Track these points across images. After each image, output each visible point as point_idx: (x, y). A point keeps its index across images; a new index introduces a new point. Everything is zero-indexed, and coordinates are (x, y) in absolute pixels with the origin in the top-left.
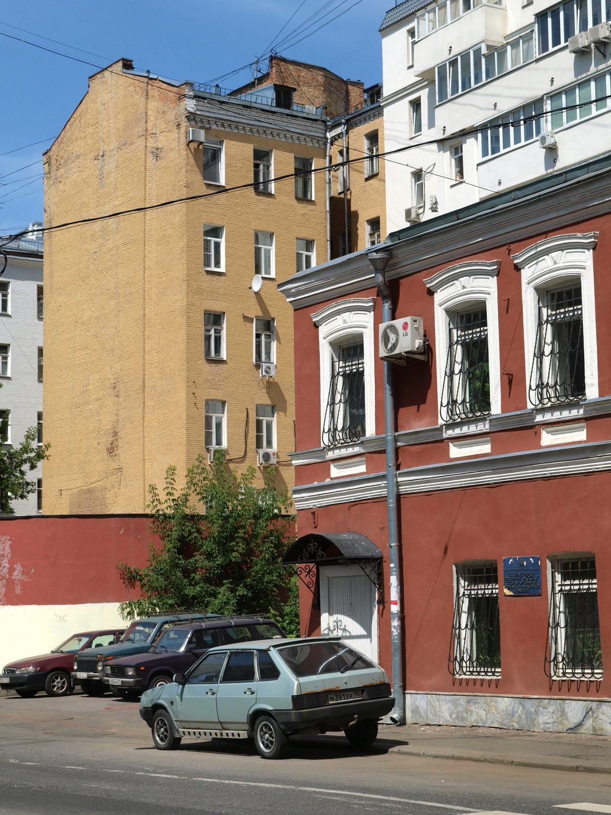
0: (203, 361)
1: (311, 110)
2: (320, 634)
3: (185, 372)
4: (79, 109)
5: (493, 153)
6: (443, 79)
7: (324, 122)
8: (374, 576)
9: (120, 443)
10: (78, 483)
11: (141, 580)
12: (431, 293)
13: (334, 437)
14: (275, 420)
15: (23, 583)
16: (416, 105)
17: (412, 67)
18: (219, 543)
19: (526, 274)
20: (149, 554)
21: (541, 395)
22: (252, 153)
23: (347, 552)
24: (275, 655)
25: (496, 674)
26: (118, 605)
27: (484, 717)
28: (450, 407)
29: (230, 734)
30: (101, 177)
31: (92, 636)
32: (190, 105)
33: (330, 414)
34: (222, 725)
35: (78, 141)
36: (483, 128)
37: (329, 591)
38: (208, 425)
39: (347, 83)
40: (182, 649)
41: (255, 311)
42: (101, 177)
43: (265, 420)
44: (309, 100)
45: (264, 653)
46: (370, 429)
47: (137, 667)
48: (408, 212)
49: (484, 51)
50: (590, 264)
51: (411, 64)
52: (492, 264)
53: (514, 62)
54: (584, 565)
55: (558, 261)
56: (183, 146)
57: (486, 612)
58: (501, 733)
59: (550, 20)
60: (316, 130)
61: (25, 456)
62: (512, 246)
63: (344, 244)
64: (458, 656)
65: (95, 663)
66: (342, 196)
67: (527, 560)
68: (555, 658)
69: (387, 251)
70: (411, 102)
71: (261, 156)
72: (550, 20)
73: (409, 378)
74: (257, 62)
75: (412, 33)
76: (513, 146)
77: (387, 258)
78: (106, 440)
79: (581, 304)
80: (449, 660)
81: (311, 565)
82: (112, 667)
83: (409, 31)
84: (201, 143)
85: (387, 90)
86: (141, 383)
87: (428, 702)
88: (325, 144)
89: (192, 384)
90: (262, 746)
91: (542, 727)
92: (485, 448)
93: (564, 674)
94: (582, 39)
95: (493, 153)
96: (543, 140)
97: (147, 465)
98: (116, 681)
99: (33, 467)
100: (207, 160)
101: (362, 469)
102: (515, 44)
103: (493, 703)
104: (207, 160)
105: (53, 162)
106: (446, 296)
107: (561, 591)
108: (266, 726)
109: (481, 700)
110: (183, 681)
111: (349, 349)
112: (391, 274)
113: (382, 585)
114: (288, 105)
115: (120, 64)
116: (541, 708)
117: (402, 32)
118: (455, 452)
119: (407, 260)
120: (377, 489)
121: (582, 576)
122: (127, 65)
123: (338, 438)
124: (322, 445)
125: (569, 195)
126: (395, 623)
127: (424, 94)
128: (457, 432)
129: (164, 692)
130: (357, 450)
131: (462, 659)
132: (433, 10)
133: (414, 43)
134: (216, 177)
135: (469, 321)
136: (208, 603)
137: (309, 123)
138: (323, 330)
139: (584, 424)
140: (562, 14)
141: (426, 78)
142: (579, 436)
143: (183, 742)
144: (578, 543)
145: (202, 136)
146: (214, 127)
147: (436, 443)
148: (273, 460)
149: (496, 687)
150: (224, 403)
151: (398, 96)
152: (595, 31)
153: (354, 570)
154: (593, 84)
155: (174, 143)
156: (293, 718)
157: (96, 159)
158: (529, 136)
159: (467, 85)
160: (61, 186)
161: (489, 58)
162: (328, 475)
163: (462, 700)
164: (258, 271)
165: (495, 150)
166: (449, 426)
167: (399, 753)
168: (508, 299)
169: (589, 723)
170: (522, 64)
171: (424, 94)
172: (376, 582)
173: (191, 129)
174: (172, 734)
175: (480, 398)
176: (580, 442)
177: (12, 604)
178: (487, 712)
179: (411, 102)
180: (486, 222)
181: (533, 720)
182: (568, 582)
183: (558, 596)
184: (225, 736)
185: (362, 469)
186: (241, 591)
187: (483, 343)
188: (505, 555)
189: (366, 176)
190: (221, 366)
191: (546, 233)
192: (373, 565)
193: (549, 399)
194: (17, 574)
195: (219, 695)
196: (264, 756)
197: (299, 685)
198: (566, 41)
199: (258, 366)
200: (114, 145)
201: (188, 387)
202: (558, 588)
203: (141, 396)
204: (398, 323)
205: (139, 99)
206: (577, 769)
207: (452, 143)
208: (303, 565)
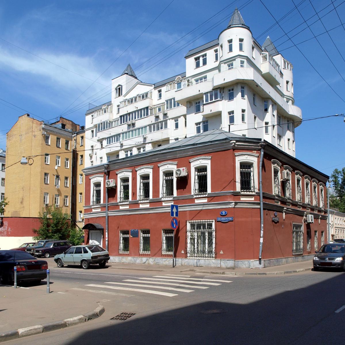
0: (44, 184)
1: (70, 130)
2: (89, 244)
3: (40, 186)
4: (16, 124)
5: (109, 144)
6: (99, 126)
7: (72, 133)
8: (102, 232)
9: (24, 201)
10: (13, 210)
11: (37, 232)
12: (117, 174)
14: (59, 198)
15: (11, 232)
16: (93, 131)
17: (92, 123)
18: (55, 225)
19: (138, 172)
20: (39, 226)
22: (56, 138)
23: (97, 227)
24: (87, 248)
25: (128, 253)
26: (32, 237)
29: (76, 264)
30: (21, 140)
31: (28, 244)
32: (43, 126)
33: (93, 199)
34: (74, 262)
35: (15, 131)
36: (108, 138)
38: (44, 198)
39: (76, 125)
40: (52, 247)
41: (56, 174)
42: (21, 140)
43: (57, 197)
44: (69, 128)
45: (84, 248)
46: (102, 202)
47: (42, 251)
49: (108, 122)
52: (131, 170)
54: (147, 231)
56: (41, 135)
57: (126, 240)
58: (129, 264)
59: (123, 117)
60: (70, 134)
61: (3, 203)
62: (135, 167)
63: (75, 160)
65: (31, 249)
66: (75, 149)
70: (91, 131)
71: (58, 139)
72: (123, 117)
73: (111, 192)
74: (57, 118)
75: (92, 116)
76: (114, 143)
78: (21, 200)
81: (88, 230)
82: (36, 251)
83: (92, 116)
84: (45, 135)
85: (86, 127)
86: (29, 188)
88: (72, 138)
89: (41, 188)
90: (84, 267)
92: (128, 207)
94: (130, 123)
95: (109, 144)
96: (120, 142)
97: (30, 206)
98: (37, 254)
99: (5, 206)
100: (46, 138)
101: (100, 210)
102: (115, 121)
104: (46, 138)
105: (9, 135)
106: (121, 175)
108: (85, 263)
110: (65, 253)
111: (98, 185)
112: (108, 170)
113: (103, 234)
114: (64, 129)
115: (27, 115)
117: (90, 116)
118: (121, 208)
119: (112, 167)
120: (104, 215)
121: (126, 234)
122: (28, 115)
125: (148, 157)
126: (107, 242)
127: (94, 129)
128: (122, 204)
129: (61, 256)
130: (99, 206)
132: (98, 112)
134: (48, 143)
135: (125, 181)
136: (53, 238)
137: (69, 133)
138: (92, 181)
139: (149, 204)
140: (125, 117)
141: (95, 126)
142: (148, 206)
143: (64, 266)
144: (146, 227)
145: (45, 133)
146: (48, 131)
147: (117, 206)
148: (58, 207)
149: (128, 255)
150: (48, 193)
151: (89, 129)
152: (132, 121)
153: (98, 231)
154: (131, 132)
155: (39, 134)
156: (91, 261)
157: (20, 136)
158: (117, 141)
160: (11, 141)
161: (109, 124)
163: (121, 258)
164: (56, 165)
165: (110, 143)
166: (120, 202)
167: (111, 268)
169: (147, 262)
170: (116, 126)
171: (94, 129)
173: (43, 132)
174: (62, 264)
175: (126, 197)
177: (8, 236)
178: (126, 260)
179: (91, 131)
180: (130, 161)
181: (136, 261)
182: (144, 235)
184: (75, 265)
185: (100, 210)
186: (60, 235)
188: (131, 229)
190: (48, 185)
191: (143, 165)
194: (9, 230)
195: (74, 256)
196: (84, 268)
197: (93, 254)
199: (56, 186)
200: (24, 133)
201: (40, 189)
202: (142, 236)
203: (29, 191)
204: (110, 180)
205: (31, 124)
206: (148, 270)
207: (101, 141)
208: (86, 230)
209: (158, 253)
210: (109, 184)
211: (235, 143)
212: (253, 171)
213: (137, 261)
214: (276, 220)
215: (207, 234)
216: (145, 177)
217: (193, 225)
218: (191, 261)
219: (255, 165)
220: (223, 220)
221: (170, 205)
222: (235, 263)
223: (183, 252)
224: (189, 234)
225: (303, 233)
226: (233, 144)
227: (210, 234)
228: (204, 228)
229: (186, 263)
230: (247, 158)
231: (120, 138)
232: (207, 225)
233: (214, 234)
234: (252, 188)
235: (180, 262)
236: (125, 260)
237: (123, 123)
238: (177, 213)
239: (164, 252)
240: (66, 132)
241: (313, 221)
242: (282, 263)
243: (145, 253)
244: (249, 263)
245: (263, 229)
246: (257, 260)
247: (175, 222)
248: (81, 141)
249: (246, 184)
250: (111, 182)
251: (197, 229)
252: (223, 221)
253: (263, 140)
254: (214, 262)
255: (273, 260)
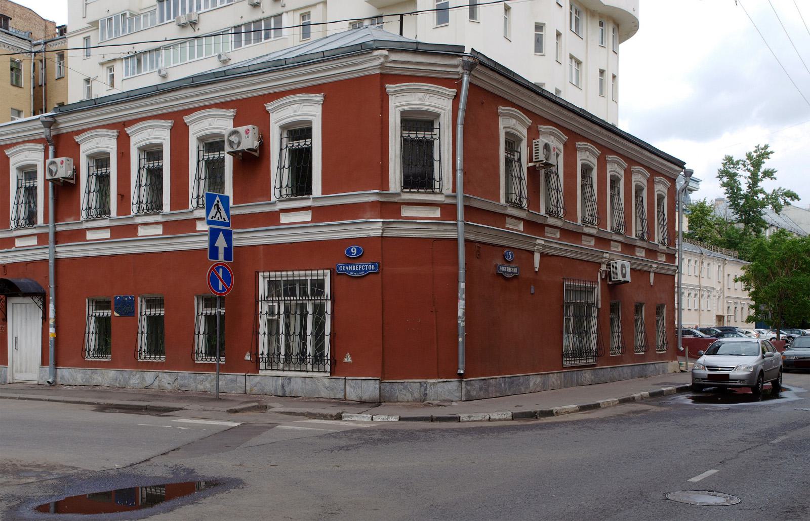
8: (40, 303)
13: (18, 223)
21: (139, 208)
25: (108, 359)
27: (100, 381)
28: (87, 211)
37: (13, 311)
48: (774, 190)
50: (168, 138)
51: (85, 16)
53: (145, 24)
55: (151, 134)
57: (104, 325)
64: (87, 348)
67: (127, 297)
68: (140, 350)
69: (52, 117)
77: (51, 121)
79: (163, 160)
80: (82, 350)
87: (70, 373)
91: (132, 385)
93: (145, 358)
103: (106, 373)
107: (145, 314)
109: (99, 372)
116: (132, 376)
123: (20, 224)
124: (10, 228)
131: (90, 350)
133: (86, 4)
159: (118, 33)
162: (14, 246)
168: (123, 153)
172: (41, 307)
176: (159, 235)
178: (103, 378)
183: (143, 317)
187: (308, 151)
189: (56, 78)
192: (40, 297)
193: (143, 210)
198: (174, 18)
204: (58, 160)
207: (109, 64)
209: (132, 362)
210: (54, 171)
211: (386, 57)
212: (439, 137)
213: (132, 382)
214: (510, 273)
215: (310, 309)
216: (152, 153)
217: (273, 284)
218: (268, 379)
219: (445, 120)
220: (352, 271)
221: (206, 231)
222: (383, 387)
223: (248, 357)
224: (263, 308)
225: (597, 307)
226: (382, 60)
227: (319, 310)
228: (304, 293)
229: (255, 388)
230: (420, 100)
231: (160, 59)
232: (311, 286)
233: (328, 307)
234: (437, 185)
235: (241, 383)
236: (100, 379)
237: (168, 19)
238: (228, 252)
239: (200, 359)
240: (10, 37)
241: (628, 278)
242: (527, 388)
243: (212, 360)
244: (422, 389)
245: (464, 296)
246: (445, 380)
247: (221, 275)
248: (57, 66)
249: (419, 177)
250: (59, 165)
251: (286, 294)
252: (352, 274)
253: (468, 51)
254: (327, 385)
255: (496, 380)
